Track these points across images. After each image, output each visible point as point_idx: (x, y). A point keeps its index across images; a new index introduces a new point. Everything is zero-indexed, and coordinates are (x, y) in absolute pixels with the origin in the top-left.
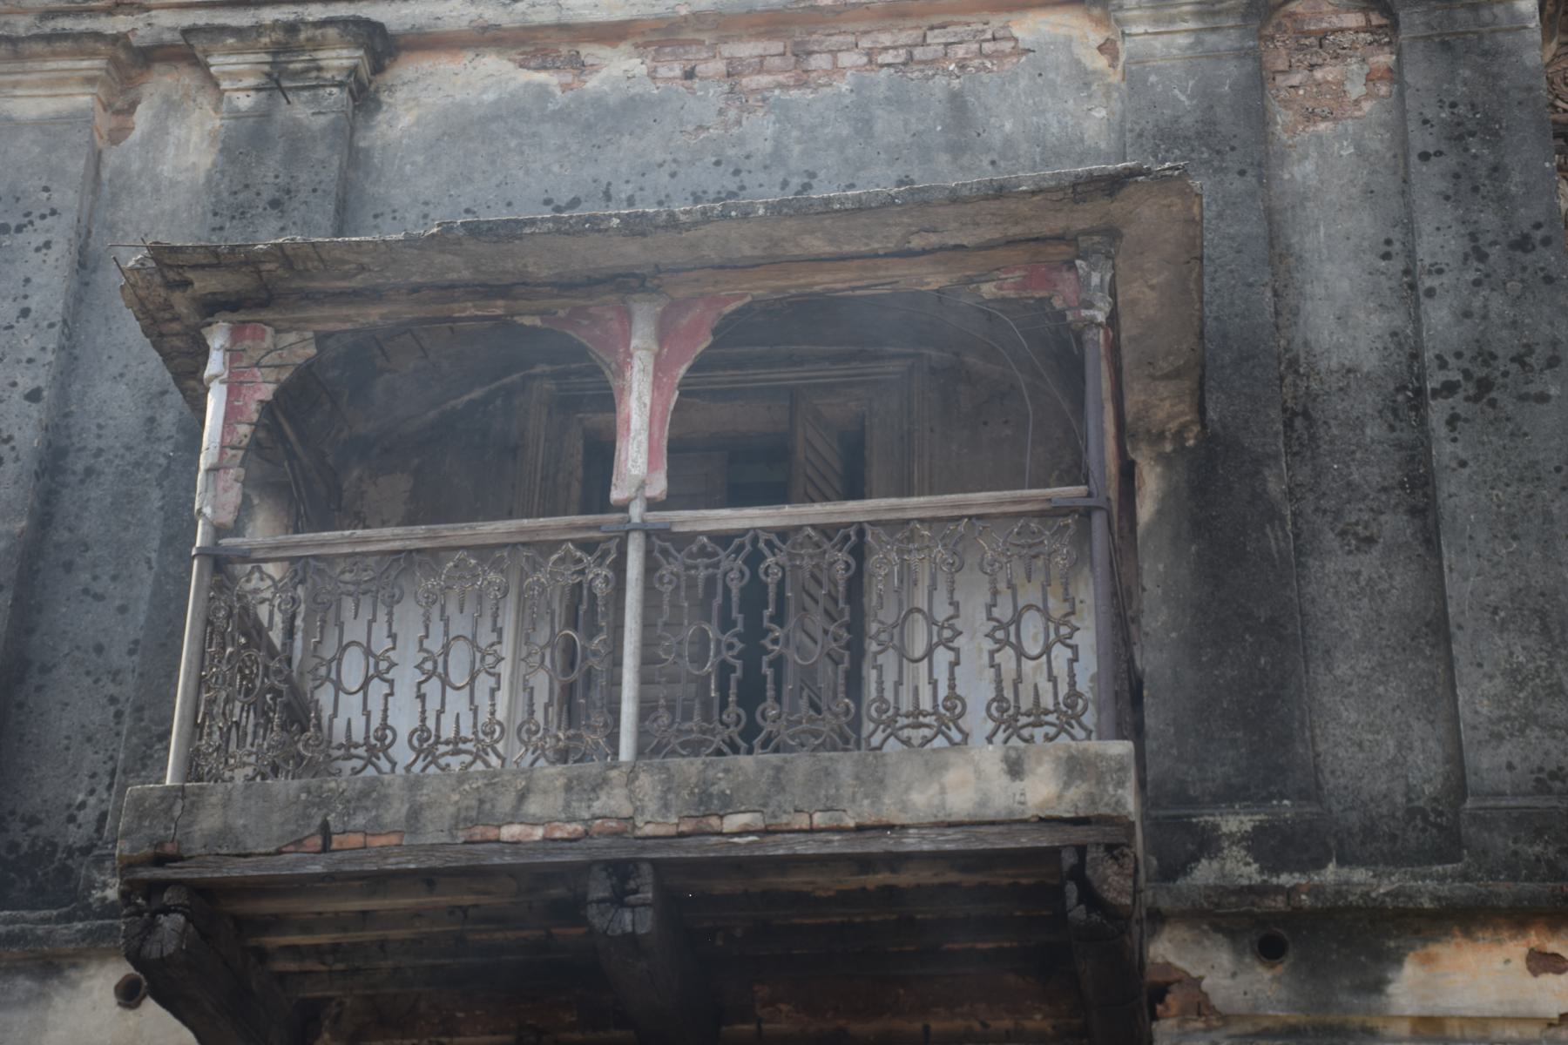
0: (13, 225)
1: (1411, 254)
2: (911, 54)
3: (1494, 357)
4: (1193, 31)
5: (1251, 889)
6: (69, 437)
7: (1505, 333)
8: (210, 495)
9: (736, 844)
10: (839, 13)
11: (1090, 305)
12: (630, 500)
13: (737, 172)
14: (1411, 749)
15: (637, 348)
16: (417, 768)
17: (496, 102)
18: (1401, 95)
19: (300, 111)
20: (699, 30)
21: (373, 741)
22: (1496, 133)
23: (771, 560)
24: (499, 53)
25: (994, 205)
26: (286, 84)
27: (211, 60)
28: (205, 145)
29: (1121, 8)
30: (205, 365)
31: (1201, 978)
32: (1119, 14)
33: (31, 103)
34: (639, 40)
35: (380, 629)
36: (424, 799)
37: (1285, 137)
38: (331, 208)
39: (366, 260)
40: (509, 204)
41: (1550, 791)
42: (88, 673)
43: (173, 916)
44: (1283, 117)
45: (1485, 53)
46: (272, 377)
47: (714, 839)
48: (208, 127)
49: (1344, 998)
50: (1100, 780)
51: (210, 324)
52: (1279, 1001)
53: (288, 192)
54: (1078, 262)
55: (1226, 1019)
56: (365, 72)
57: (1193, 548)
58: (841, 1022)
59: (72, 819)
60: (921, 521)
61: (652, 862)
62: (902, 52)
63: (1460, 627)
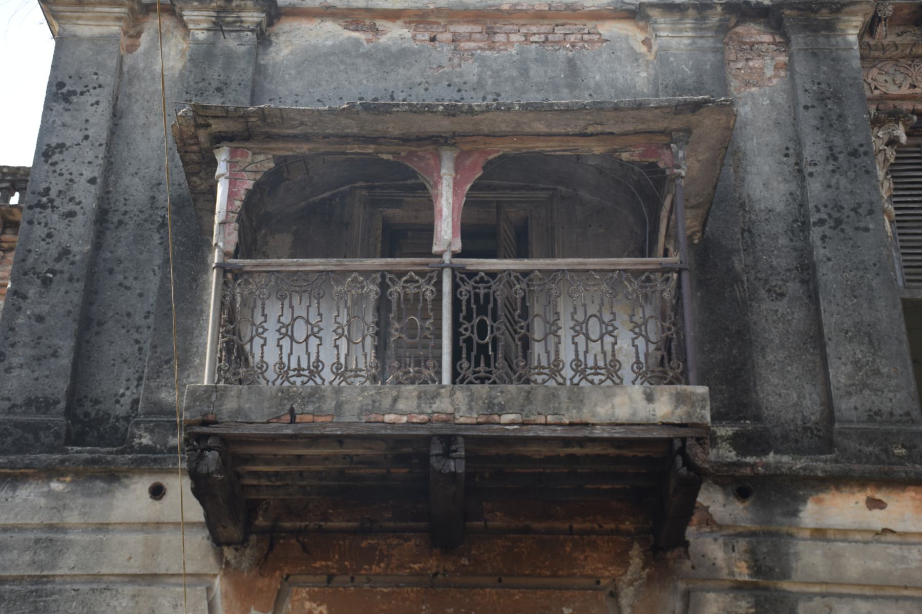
0: (79, 92)
1: (799, 155)
2: (547, 38)
3: (843, 208)
4: (691, 37)
5: (733, 464)
6: (109, 204)
7: (847, 197)
8: (222, 236)
9: (508, 430)
10: (511, 14)
11: (679, 167)
12: (444, 252)
13: (459, 91)
14: (804, 398)
15: (445, 174)
16: (335, 383)
17: (333, 46)
18: (792, 77)
19: (231, 42)
20: (437, 17)
21: (312, 368)
22: (840, 99)
23: (518, 286)
24: (333, 21)
25: (634, 113)
26: (224, 28)
27: (184, 13)
28: (178, 57)
29: (656, 22)
30: (215, 171)
31: (708, 507)
32: (655, 26)
33: (86, 28)
34: (407, 20)
35: (313, 311)
36: (344, 399)
37: (735, 93)
38: (249, 94)
39: (305, 119)
40: (341, 99)
41: (875, 421)
42: (123, 327)
43: (213, 452)
44: (734, 83)
45: (833, 60)
46: (252, 177)
47: (496, 426)
48: (180, 47)
49: (778, 518)
50: (693, 405)
51: (218, 148)
52: (747, 519)
53: (226, 84)
54: (672, 145)
55: (721, 527)
56: (264, 25)
57: (699, 294)
58: (528, 522)
59: (117, 402)
60: (595, 271)
61: (464, 436)
62: (542, 36)
63: (830, 339)
